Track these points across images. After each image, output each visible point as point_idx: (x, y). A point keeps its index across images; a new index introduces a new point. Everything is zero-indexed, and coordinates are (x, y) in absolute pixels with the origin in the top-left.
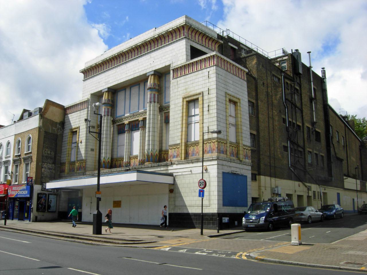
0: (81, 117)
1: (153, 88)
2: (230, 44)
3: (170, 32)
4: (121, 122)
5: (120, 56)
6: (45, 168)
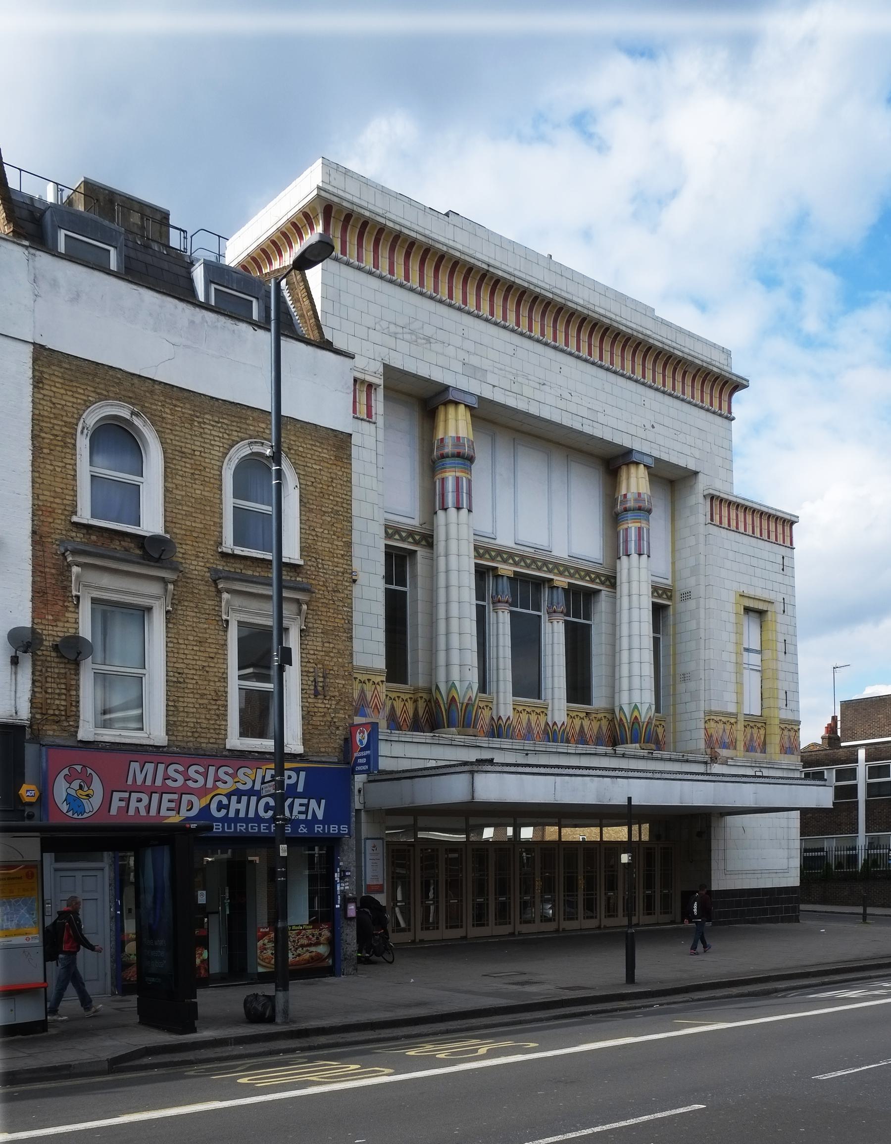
1: (453, 456)
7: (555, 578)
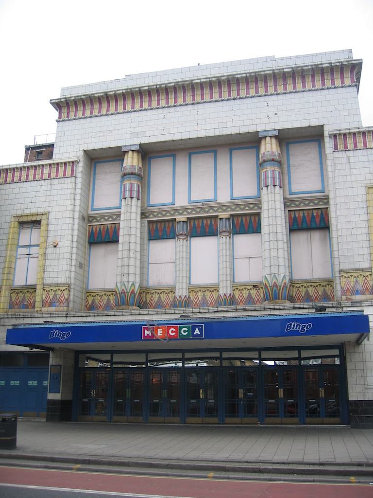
1: (277, 162)
7: (219, 214)
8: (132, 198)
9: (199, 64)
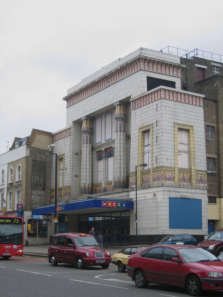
0: (66, 144)
2: (196, 65)
3: (129, 64)
4: (99, 149)
5: (104, 79)
6: (35, 195)
7: (112, 146)
8: (87, 143)
9: (103, 67)
